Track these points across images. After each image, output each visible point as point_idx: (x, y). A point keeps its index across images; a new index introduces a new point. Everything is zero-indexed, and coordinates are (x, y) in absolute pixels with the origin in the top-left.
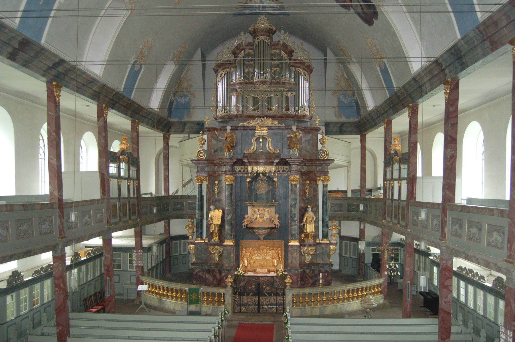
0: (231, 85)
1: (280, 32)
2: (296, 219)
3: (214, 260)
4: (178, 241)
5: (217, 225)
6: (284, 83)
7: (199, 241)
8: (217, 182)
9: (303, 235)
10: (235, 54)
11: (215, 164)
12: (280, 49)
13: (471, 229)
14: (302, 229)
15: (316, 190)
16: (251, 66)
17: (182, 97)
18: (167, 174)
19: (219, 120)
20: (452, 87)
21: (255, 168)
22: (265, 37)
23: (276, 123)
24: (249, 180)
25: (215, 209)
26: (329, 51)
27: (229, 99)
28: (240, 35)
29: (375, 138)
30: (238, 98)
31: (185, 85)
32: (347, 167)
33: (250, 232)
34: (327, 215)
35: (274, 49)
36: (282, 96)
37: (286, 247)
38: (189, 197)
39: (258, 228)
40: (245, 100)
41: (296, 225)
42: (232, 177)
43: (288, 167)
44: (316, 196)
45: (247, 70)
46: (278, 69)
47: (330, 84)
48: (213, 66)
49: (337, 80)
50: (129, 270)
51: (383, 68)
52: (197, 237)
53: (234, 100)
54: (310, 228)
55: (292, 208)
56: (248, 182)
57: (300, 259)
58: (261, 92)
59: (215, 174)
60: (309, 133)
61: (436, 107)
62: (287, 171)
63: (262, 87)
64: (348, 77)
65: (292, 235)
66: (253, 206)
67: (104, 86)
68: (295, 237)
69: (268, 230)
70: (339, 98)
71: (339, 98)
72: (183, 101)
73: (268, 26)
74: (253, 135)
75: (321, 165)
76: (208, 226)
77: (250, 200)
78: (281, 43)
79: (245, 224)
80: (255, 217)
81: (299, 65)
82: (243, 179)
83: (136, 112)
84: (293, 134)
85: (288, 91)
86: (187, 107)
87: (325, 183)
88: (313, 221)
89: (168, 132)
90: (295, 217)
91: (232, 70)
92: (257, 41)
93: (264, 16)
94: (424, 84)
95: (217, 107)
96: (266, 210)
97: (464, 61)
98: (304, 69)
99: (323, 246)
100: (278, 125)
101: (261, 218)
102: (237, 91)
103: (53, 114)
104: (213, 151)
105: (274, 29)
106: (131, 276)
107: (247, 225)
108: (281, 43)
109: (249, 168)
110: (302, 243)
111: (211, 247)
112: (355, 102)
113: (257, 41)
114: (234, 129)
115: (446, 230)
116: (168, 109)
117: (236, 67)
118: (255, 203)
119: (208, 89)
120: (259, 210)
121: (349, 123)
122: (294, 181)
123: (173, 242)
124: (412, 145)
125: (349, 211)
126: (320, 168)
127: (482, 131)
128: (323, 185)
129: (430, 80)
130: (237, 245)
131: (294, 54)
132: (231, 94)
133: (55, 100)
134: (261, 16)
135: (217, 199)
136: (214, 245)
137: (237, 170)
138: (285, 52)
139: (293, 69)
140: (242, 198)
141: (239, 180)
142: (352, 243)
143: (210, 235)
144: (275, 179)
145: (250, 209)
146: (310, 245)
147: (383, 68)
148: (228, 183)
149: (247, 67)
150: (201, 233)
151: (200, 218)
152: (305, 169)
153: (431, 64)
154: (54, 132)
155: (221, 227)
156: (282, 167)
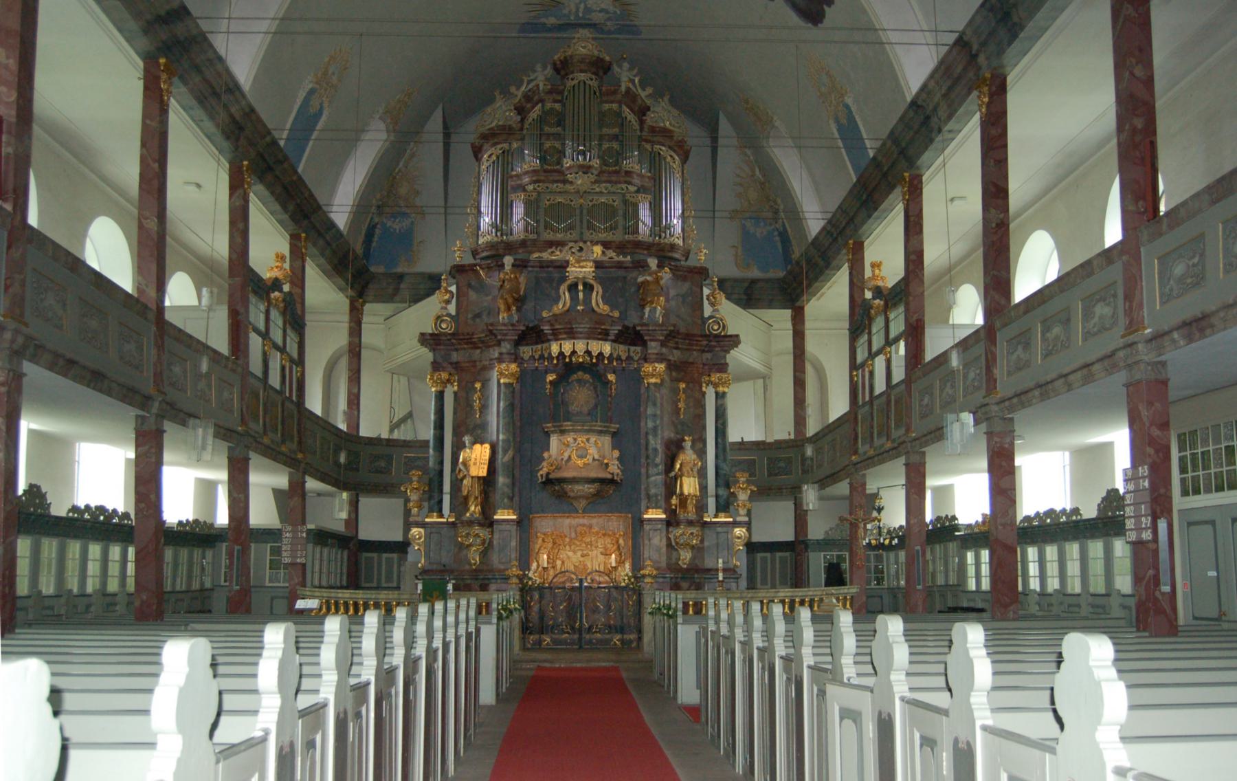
0: (512, 177)
1: (620, 67)
2: (658, 460)
3: (470, 564)
4: (375, 555)
5: (479, 478)
6: (628, 173)
7: (434, 519)
8: (478, 385)
9: (674, 501)
10: (521, 111)
11: (474, 343)
12: (620, 103)
13: (1048, 335)
14: (670, 487)
15: (701, 405)
16: (557, 137)
17: (395, 218)
18: (355, 391)
19: (485, 254)
20: (994, 89)
21: (567, 347)
22: (589, 75)
23: (611, 253)
24: (551, 377)
25: (474, 443)
26: (724, 126)
27: (505, 210)
28: (535, 71)
29: (831, 300)
30: (528, 204)
31: (403, 190)
32: (764, 378)
33: (556, 490)
34: (725, 460)
35: (606, 102)
36: (625, 202)
37: (639, 523)
38: (406, 444)
39: (574, 480)
40: (542, 211)
41: (658, 474)
42: (513, 367)
43: (639, 349)
44: (701, 416)
45: (548, 145)
46: (615, 145)
47: (727, 198)
48: (472, 138)
49: (741, 185)
50: (267, 584)
51: (844, 121)
52: (431, 510)
53: (519, 211)
54: (689, 486)
55: (650, 437)
56: (551, 382)
57: (669, 558)
58: (578, 192)
59: (475, 366)
60: (684, 279)
61: (956, 202)
62: (636, 358)
63: (581, 181)
64: (764, 176)
65: (649, 497)
66: (563, 432)
67: (251, 112)
68: (657, 501)
69: (596, 485)
70: (744, 227)
71: (744, 227)
72: (397, 226)
73: (596, 53)
74: (563, 279)
75: (710, 349)
76: (456, 484)
77: (554, 418)
78: (623, 89)
79: (544, 471)
80: (566, 455)
81: (661, 139)
82: (539, 375)
83: (303, 213)
84: (650, 275)
85: (638, 191)
86: (406, 240)
87: (721, 389)
88: (695, 470)
89: (361, 294)
90: (656, 456)
91: (515, 145)
92: (570, 84)
93: (584, 32)
94: (935, 109)
95: (479, 227)
96: (593, 439)
97: (1015, 19)
98: (670, 147)
99: (719, 529)
100: (616, 259)
101: (581, 457)
102: (524, 190)
103: (154, 124)
104: (470, 316)
105: (607, 58)
106: (272, 599)
107: (548, 474)
108: (623, 89)
109: (555, 348)
110: (671, 521)
111: (463, 531)
112: (780, 234)
113: (570, 84)
114: (520, 265)
115: (997, 372)
116: (366, 236)
117: (523, 139)
118: (567, 425)
119: (457, 206)
120: (575, 439)
121: (767, 281)
122: (653, 376)
123: (365, 555)
124: (913, 257)
125: (770, 475)
126: (709, 355)
127: (1055, 254)
128: (717, 393)
129: (945, 96)
130: (523, 523)
131: (650, 115)
132: (512, 196)
133: (162, 96)
134: (581, 31)
135: (479, 422)
136: (470, 523)
137: (526, 357)
138: (632, 110)
139: (648, 146)
140: (533, 416)
141: (527, 379)
142: (778, 555)
143: (460, 503)
144: (611, 377)
145: (554, 441)
146: (690, 523)
147: (844, 121)
148: (507, 381)
149: (548, 139)
150: (440, 502)
151: (437, 467)
152: (676, 355)
153: (949, 52)
154: (155, 161)
155: (487, 482)
156: (626, 348)
